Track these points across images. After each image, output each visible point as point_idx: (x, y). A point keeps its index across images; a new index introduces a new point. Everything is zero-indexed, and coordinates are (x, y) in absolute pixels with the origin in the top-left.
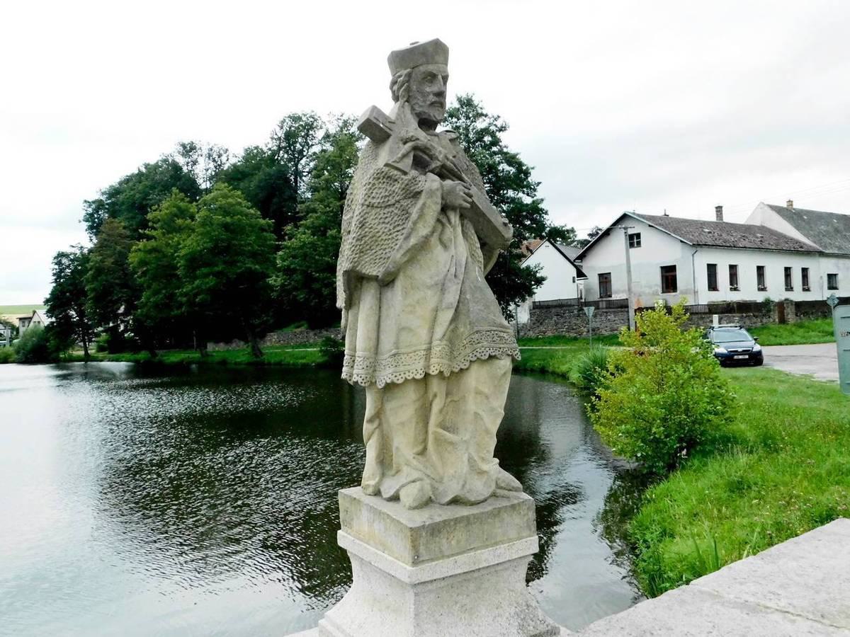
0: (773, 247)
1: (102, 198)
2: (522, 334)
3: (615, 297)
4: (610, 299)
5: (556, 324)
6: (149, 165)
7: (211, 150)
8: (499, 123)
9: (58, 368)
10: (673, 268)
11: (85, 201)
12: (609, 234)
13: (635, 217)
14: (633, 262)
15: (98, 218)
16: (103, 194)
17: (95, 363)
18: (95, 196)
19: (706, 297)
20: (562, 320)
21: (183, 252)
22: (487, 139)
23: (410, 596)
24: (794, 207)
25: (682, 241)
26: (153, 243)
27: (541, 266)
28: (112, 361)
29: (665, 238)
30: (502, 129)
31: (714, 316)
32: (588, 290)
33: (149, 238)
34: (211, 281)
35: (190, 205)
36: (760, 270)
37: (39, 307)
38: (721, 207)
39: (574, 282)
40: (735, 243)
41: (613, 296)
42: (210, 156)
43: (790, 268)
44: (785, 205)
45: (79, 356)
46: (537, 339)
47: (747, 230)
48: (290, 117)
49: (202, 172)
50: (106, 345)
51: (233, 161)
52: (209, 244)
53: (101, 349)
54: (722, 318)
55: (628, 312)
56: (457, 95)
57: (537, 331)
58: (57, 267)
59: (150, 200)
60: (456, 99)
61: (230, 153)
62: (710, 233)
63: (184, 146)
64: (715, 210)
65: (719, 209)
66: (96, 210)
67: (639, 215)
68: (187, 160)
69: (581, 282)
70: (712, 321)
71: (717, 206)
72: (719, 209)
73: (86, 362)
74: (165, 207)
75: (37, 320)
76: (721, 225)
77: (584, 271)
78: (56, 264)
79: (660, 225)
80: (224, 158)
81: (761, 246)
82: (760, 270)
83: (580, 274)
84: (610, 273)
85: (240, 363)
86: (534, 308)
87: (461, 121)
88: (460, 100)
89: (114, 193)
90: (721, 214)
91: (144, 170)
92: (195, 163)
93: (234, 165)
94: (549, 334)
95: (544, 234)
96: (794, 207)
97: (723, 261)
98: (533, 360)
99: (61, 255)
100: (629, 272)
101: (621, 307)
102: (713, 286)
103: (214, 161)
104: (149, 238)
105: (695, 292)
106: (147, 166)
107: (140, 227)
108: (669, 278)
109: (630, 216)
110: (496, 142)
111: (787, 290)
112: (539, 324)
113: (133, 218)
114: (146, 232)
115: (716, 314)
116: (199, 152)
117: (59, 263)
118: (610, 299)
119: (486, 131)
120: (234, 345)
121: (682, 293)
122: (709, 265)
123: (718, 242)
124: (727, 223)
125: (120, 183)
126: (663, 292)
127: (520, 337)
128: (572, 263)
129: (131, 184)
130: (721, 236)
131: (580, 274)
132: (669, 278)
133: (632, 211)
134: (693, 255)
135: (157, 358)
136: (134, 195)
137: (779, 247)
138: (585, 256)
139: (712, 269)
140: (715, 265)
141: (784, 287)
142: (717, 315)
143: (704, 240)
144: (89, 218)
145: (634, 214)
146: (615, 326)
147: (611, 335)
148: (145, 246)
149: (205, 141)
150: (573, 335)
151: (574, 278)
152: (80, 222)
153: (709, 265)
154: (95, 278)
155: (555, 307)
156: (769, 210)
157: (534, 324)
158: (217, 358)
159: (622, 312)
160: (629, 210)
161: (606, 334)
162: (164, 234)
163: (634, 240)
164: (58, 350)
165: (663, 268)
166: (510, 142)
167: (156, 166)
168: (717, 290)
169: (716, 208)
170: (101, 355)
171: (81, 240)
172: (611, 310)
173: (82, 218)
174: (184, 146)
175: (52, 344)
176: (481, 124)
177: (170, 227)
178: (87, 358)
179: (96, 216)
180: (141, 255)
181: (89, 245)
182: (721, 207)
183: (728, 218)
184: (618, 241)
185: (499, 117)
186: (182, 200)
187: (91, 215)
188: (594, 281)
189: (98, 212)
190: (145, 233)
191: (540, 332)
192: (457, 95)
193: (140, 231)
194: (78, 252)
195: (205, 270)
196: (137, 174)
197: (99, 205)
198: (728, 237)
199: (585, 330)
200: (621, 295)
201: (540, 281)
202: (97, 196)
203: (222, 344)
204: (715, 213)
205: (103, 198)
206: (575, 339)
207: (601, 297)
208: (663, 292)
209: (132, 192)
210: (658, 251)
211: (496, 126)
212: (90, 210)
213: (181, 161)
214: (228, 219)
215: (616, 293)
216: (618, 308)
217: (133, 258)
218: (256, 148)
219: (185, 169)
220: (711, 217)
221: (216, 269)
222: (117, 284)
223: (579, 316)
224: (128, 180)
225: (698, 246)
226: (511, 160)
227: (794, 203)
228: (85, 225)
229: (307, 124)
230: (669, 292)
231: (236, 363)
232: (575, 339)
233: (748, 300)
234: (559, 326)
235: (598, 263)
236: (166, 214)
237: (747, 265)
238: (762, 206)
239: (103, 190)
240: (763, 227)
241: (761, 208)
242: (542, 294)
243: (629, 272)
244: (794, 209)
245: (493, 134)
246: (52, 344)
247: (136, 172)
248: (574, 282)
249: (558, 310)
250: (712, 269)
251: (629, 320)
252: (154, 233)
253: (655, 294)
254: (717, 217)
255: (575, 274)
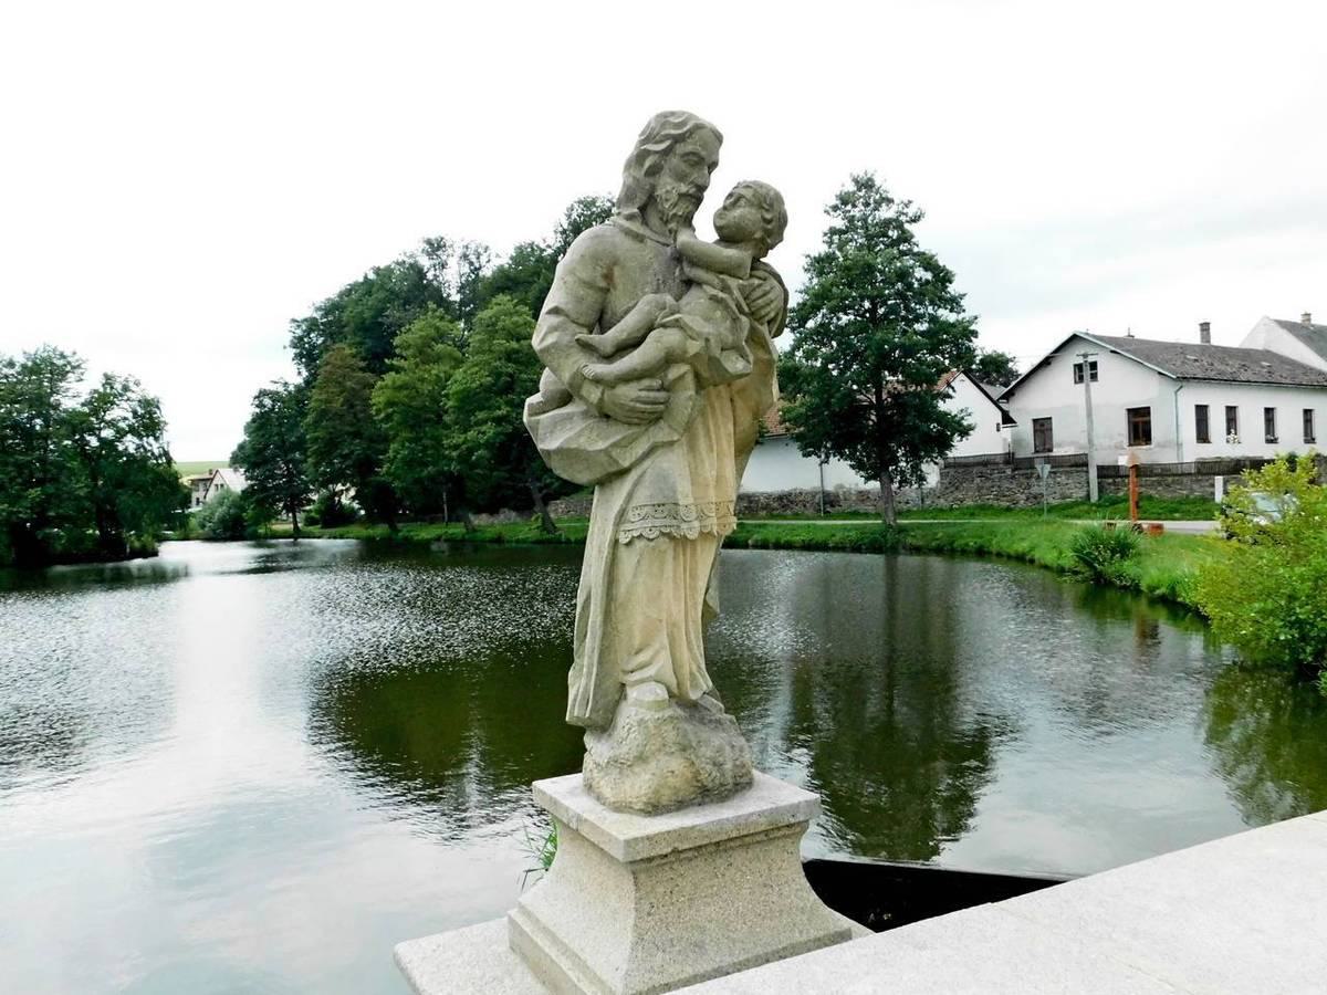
0: (1287, 381)
1: (315, 315)
2: (928, 502)
3: (1057, 452)
4: (1051, 454)
5: (979, 489)
6: (379, 269)
7: (467, 248)
8: (911, 211)
9: (259, 546)
10: (1146, 411)
11: (294, 321)
12: (1049, 364)
13: (1091, 339)
14: (1094, 401)
15: (308, 343)
16: (318, 309)
17: (307, 540)
18: (308, 312)
19: (1193, 452)
20: (988, 484)
21: (455, 388)
22: (894, 234)
23: (620, 897)
24: (1313, 322)
25: (1160, 373)
26: (402, 378)
27: (969, 411)
28: (335, 538)
29: (1139, 371)
30: (915, 220)
31: (1216, 477)
32: (1017, 442)
33: (398, 370)
34: (490, 430)
35: (451, 326)
36: (1269, 412)
37: (222, 464)
38: (1208, 324)
39: (998, 430)
40: (1235, 375)
41: (1055, 450)
42: (465, 257)
43: (1310, 411)
44: (1298, 319)
45: (286, 532)
46: (951, 509)
47: (1245, 356)
48: (580, 202)
49: (452, 279)
50: (317, 516)
51: (496, 263)
52: (489, 379)
53: (310, 521)
54: (1228, 481)
55: (1087, 472)
56: (851, 174)
57: (951, 499)
58: (258, 410)
59: (387, 316)
60: (850, 180)
61: (492, 251)
62: (1196, 360)
63: (429, 242)
64: (1199, 328)
65: (1205, 327)
66: (308, 332)
67: (1094, 336)
68: (432, 262)
69: (1007, 432)
70: (1213, 486)
71: (1202, 322)
72: (1205, 327)
73: (296, 539)
74: (414, 332)
75: (219, 483)
76: (1207, 350)
77: (1011, 415)
78: (257, 406)
79: (1128, 351)
80: (483, 259)
81: (1270, 379)
82: (1269, 412)
83: (1007, 419)
84: (1050, 418)
85: (524, 541)
86: (946, 467)
87: (857, 209)
88: (856, 181)
89: (332, 308)
90: (1209, 333)
91: (372, 276)
92: (443, 266)
93: (501, 269)
94: (969, 502)
95: (974, 367)
96: (1313, 322)
97: (1217, 400)
98: (962, 537)
99: (263, 393)
100: (1089, 415)
101: (1076, 465)
102: (1203, 436)
103: (471, 263)
104: (398, 370)
105: (1179, 445)
106: (377, 271)
107: (378, 356)
108: (1140, 425)
109: (1081, 338)
110: (906, 237)
111: (1307, 442)
112: (953, 489)
113: (361, 343)
114: (394, 362)
115: (1219, 474)
116: (450, 251)
117: (261, 405)
118: (1051, 454)
119: (887, 223)
120: (502, 516)
121: (1159, 445)
122: (1197, 406)
123: (1212, 374)
124: (1216, 347)
125: (341, 295)
126: (1130, 445)
127: (926, 506)
128: (996, 403)
129: (354, 296)
130: (1212, 365)
131: (1007, 419)
132: (1140, 425)
133: (1084, 331)
134: (1176, 393)
135: (400, 534)
136: (362, 312)
137: (1297, 381)
138: (1013, 394)
139: (1202, 411)
140: (1206, 407)
141: (1302, 438)
142: (1221, 478)
143: (1191, 370)
144: (298, 342)
145: (1087, 334)
146: (1068, 492)
147: (1061, 504)
148: (394, 382)
149: (458, 236)
150: (1005, 504)
151: (998, 424)
152: (285, 347)
153: (1197, 406)
154: (316, 423)
155: (978, 464)
156: (1274, 324)
157: (947, 488)
158: (490, 533)
159: (1078, 472)
160: (1080, 330)
161: (1055, 502)
162: (417, 365)
163: (1086, 372)
164: (257, 522)
165: (1129, 410)
166: (925, 238)
167: (389, 270)
168: (1209, 442)
169: (1201, 325)
170: (315, 529)
171: (289, 373)
172: (1061, 470)
173: (288, 343)
174: (429, 242)
175: (248, 514)
176: (886, 213)
177: (424, 354)
178: (297, 534)
179: (306, 340)
180: (388, 392)
181: (299, 380)
182: (1208, 324)
183: (1219, 339)
184: (1064, 371)
185: (910, 202)
186: (442, 318)
187: (300, 339)
188: (1026, 429)
189: (309, 334)
190: (392, 364)
191: (956, 499)
192: (851, 174)
193: (386, 361)
194: (281, 389)
195: (481, 415)
196: (362, 284)
197: (312, 324)
198: (1223, 368)
199: (1024, 497)
200: (1066, 449)
201: (965, 432)
202: (309, 313)
203: (484, 516)
204: (1199, 333)
205: (317, 315)
206: (1008, 509)
207: (1036, 452)
208: (1130, 445)
209: (360, 308)
210: (1122, 387)
211: (906, 214)
212: (299, 332)
213: (425, 262)
214: (514, 345)
215: (1059, 446)
216: (1072, 466)
217: (378, 398)
218: (531, 245)
219: (430, 276)
220: (1194, 338)
221: (499, 413)
222: (349, 433)
223: (1013, 477)
224: (350, 290)
225: (1184, 379)
226: (928, 263)
227: (1312, 317)
228: (292, 352)
229: (604, 211)
230: (1140, 445)
231: (518, 541)
232: (1008, 509)
233: (1206, 457)
234: (984, 491)
235: (1029, 406)
236: (421, 337)
237: (1251, 405)
238: (1267, 322)
239: (318, 305)
240: (1268, 352)
241: (1265, 325)
242: (961, 449)
243: (1089, 415)
244: (1313, 326)
245: (900, 226)
246: (248, 514)
247: (361, 280)
248: (998, 430)
249: (984, 469)
250: (1202, 411)
251: (1088, 483)
252: (402, 363)
253: (1119, 447)
254: (1203, 338)
255: (1000, 421)
